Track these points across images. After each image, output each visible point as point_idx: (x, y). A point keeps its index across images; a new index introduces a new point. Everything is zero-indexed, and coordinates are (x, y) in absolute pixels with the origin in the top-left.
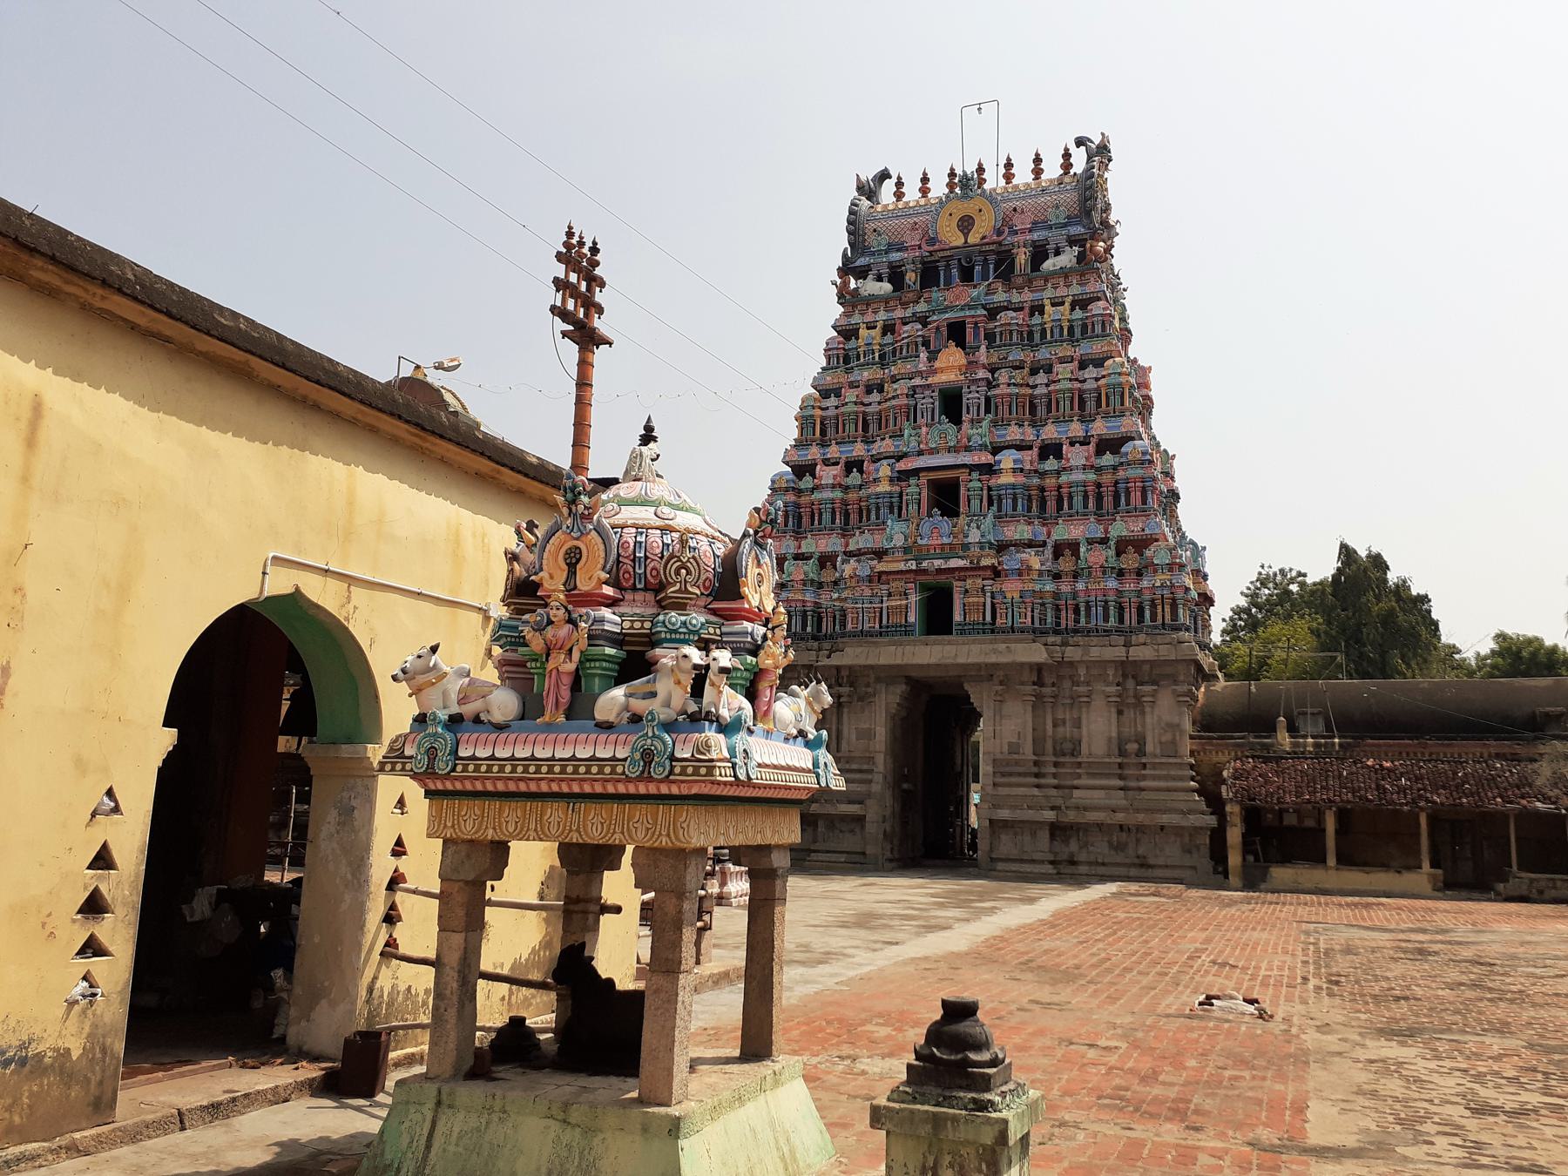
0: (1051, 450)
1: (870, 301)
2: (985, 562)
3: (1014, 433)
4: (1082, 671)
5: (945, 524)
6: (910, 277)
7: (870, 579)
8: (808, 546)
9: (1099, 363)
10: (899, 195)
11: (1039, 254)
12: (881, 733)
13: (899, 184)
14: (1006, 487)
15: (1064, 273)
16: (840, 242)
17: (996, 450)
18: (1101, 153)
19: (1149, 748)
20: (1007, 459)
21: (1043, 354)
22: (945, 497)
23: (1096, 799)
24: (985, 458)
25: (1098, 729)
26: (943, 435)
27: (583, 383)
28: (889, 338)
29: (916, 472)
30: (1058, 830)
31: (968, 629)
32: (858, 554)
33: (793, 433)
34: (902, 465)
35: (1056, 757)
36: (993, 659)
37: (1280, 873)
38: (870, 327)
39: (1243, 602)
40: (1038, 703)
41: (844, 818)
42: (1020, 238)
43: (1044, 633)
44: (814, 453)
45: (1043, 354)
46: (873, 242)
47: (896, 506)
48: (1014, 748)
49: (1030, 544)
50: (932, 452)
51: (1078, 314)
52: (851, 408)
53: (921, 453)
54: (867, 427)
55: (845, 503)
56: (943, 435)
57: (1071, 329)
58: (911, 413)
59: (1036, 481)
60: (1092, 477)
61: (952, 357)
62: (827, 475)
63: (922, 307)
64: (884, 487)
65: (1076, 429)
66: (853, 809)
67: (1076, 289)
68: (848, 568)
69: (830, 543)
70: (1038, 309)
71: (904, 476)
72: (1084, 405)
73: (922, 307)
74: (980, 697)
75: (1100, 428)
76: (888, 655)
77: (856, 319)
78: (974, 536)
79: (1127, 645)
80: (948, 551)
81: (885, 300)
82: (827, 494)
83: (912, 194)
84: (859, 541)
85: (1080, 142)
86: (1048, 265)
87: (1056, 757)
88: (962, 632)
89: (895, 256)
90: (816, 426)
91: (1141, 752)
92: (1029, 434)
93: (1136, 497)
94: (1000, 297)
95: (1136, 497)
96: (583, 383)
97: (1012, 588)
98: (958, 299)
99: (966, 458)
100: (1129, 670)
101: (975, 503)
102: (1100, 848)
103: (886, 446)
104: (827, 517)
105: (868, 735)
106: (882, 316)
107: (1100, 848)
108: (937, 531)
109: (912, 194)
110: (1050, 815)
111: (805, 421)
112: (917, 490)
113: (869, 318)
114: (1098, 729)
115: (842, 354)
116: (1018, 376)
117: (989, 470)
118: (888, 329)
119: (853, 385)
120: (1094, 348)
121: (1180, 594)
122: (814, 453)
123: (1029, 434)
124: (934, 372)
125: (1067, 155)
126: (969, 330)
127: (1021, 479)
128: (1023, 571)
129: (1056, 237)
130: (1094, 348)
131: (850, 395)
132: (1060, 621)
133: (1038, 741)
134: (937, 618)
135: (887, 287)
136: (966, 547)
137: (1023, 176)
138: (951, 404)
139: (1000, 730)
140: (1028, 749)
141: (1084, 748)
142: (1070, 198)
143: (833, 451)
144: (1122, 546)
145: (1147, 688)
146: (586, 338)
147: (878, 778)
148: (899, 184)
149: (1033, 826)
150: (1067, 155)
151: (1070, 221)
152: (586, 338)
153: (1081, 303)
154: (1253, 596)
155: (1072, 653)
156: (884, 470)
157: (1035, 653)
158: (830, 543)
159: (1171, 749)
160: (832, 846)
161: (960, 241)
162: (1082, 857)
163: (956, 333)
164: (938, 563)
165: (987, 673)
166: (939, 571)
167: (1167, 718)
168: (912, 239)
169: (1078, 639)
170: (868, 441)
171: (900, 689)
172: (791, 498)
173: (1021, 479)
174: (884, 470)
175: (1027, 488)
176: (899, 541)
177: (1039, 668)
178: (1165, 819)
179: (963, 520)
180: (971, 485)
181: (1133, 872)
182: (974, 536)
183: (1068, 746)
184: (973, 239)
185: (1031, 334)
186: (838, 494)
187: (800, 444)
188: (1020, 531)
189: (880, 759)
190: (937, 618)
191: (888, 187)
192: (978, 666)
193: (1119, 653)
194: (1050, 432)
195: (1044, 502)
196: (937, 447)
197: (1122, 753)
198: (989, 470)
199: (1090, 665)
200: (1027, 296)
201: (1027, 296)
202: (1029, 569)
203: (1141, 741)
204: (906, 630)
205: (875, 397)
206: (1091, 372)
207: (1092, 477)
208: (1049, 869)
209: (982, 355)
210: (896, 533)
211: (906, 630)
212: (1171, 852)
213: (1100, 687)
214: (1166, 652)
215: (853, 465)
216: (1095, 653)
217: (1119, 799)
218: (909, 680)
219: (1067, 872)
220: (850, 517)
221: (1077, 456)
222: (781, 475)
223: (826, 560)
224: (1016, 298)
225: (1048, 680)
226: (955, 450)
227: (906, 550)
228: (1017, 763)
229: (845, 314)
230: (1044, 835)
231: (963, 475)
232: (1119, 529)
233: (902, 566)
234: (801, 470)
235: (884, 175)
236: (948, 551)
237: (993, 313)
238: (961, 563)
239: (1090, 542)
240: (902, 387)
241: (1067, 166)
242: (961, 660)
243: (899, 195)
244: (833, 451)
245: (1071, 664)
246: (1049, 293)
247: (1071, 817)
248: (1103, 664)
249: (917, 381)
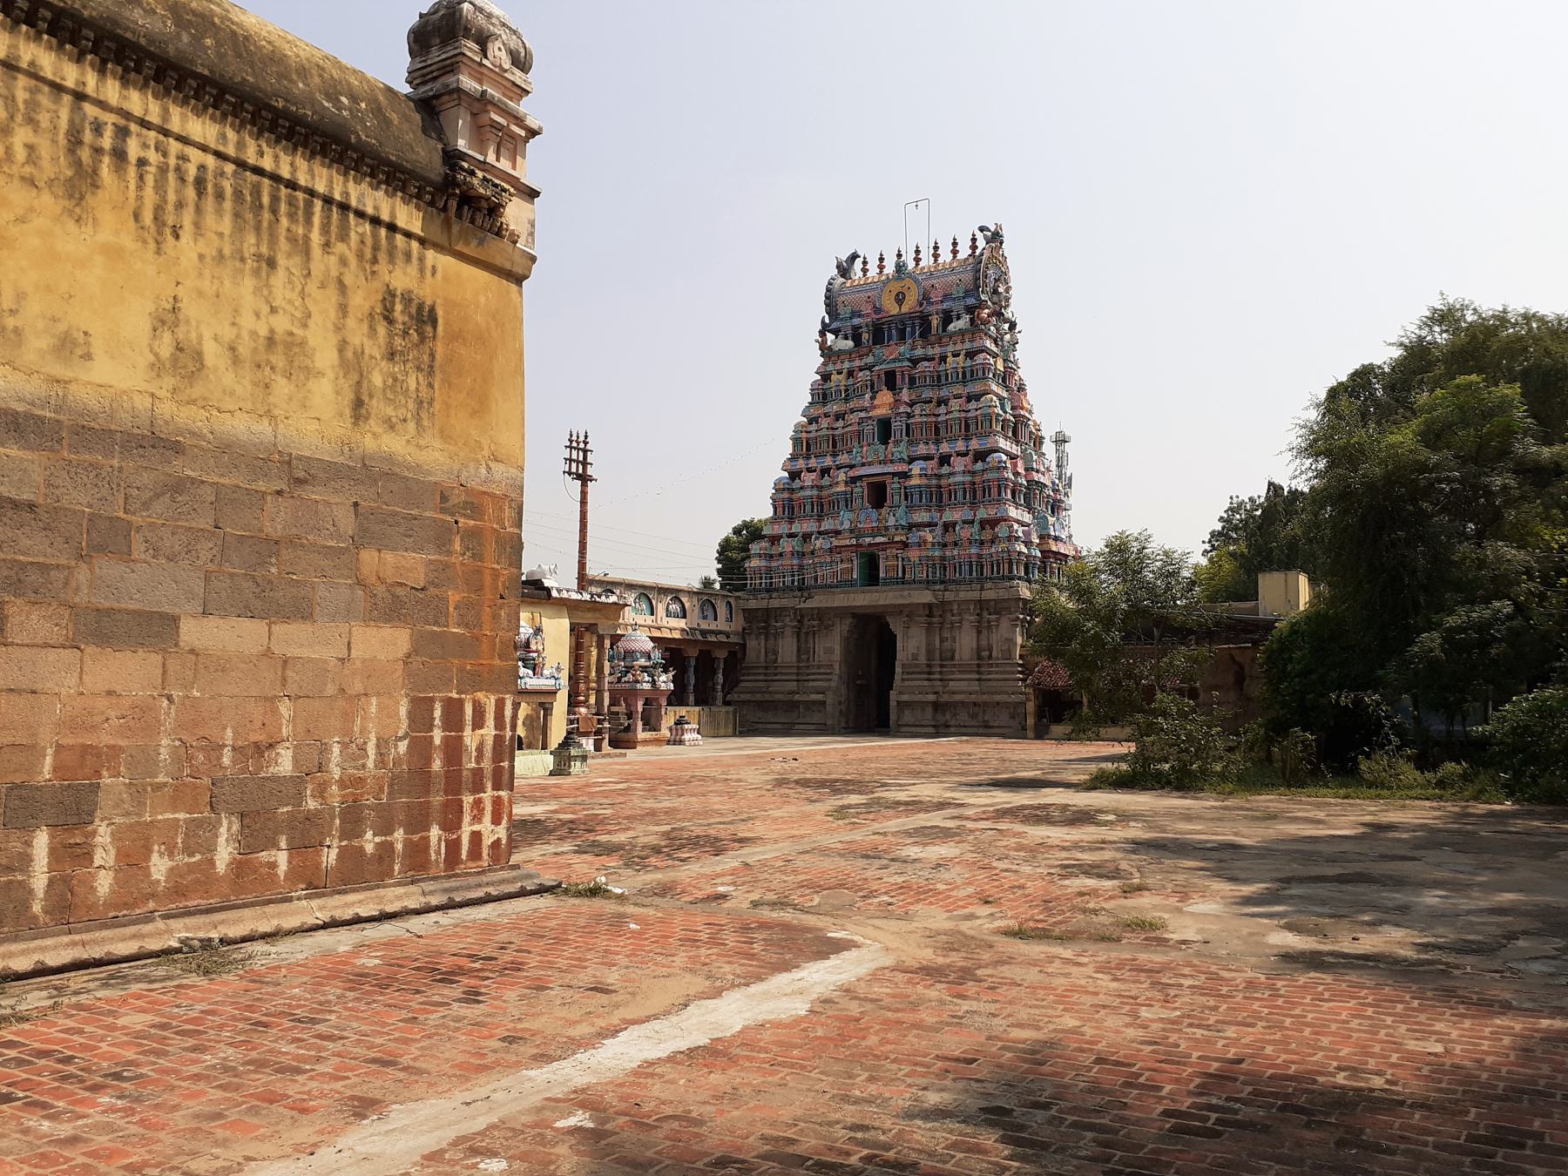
0: (944, 460)
1: (840, 353)
2: (897, 539)
3: (922, 449)
4: (955, 607)
5: (874, 514)
6: (865, 336)
7: (831, 550)
8: (796, 528)
9: (978, 397)
10: (865, 271)
11: (947, 318)
12: (838, 649)
13: (865, 263)
14: (915, 487)
15: (962, 332)
16: (821, 312)
17: (912, 460)
18: (995, 238)
19: (994, 654)
20: (916, 469)
21: (944, 393)
22: (878, 495)
23: (962, 687)
24: (903, 468)
25: (965, 643)
26: (876, 453)
27: (583, 502)
28: (851, 381)
29: (860, 478)
30: (937, 706)
31: (890, 582)
32: (826, 533)
33: (788, 449)
34: (851, 473)
35: (940, 661)
36: (900, 601)
37: (1057, 729)
38: (839, 373)
39: (1218, 526)
40: (929, 628)
41: (814, 702)
42: (932, 309)
43: (935, 583)
44: (801, 464)
45: (944, 393)
46: (844, 312)
47: (848, 501)
48: (915, 656)
49: (929, 525)
50: (870, 464)
51: (969, 363)
52: (825, 432)
53: (863, 465)
54: (835, 445)
55: (819, 497)
56: (876, 453)
57: (964, 373)
58: (859, 435)
59: (934, 482)
60: (968, 478)
61: (885, 397)
62: (808, 479)
63: (870, 359)
64: (841, 488)
65: (960, 446)
66: (820, 697)
67: (967, 345)
68: (819, 543)
69: (810, 526)
70: (943, 359)
71: (854, 480)
72: (968, 428)
73: (870, 359)
74: (896, 626)
75: (975, 444)
76: (840, 600)
77: (830, 367)
78: (891, 521)
79: (982, 589)
80: (875, 532)
81: (849, 352)
82: (808, 493)
83: (873, 270)
84: (827, 525)
85: (982, 229)
86: (951, 327)
87: (940, 661)
88: (885, 584)
89: (856, 321)
90: (804, 445)
91: (990, 657)
92: (932, 449)
93: (994, 491)
94: (919, 352)
95: (994, 491)
96: (583, 502)
97: (914, 554)
98: (893, 354)
99: (890, 469)
100: (981, 604)
101: (896, 498)
102: (963, 717)
103: (843, 459)
104: (808, 507)
105: (830, 651)
106: (847, 365)
107: (963, 717)
108: (868, 518)
109: (873, 270)
110: (931, 697)
111: (796, 441)
112: (860, 489)
113: (838, 367)
114: (965, 643)
115: (821, 395)
116: (928, 408)
117: (905, 475)
118: (850, 374)
119: (826, 415)
120: (975, 388)
121: (1015, 556)
122: (801, 464)
123: (932, 449)
124: (874, 407)
125: (974, 240)
126: (898, 376)
127: (925, 481)
128: (922, 543)
129: (958, 307)
130: (975, 388)
131: (824, 423)
132: (942, 574)
133: (930, 652)
134: (871, 575)
135: (850, 343)
136: (887, 528)
137: (946, 256)
138: (885, 427)
139: (910, 645)
140: (923, 660)
141: (957, 656)
142: (968, 277)
143: (813, 463)
144: (983, 524)
145: (993, 617)
146: (584, 479)
147: (835, 678)
148: (865, 263)
149: (923, 704)
150: (974, 240)
151: (967, 294)
152: (584, 479)
153: (971, 355)
154: (1226, 521)
155: (949, 596)
156: (842, 476)
157: (926, 597)
158: (810, 526)
159: (1008, 654)
160: (808, 720)
161: (895, 311)
162: (952, 723)
163: (890, 381)
164: (868, 540)
165: (899, 610)
166: (870, 545)
167: (1006, 635)
168: (867, 309)
169: (952, 587)
170: (834, 455)
171: (849, 621)
172: (786, 495)
173: (925, 481)
174: (842, 476)
175: (928, 486)
176: (847, 525)
177: (930, 606)
178: (998, 698)
179: (884, 511)
180: (893, 486)
181: (981, 731)
182: (891, 521)
183: (949, 654)
184: (905, 309)
185: (939, 377)
186: (815, 492)
187: (793, 458)
188: (922, 516)
189: (837, 666)
190: (871, 575)
191: (858, 264)
192: (894, 606)
193: (975, 595)
194: (945, 448)
195: (938, 496)
196: (872, 461)
197: (980, 658)
198: (905, 475)
199: (960, 603)
200: (936, 351)
201: (936, 351)
202: (925, 542)
203: (990, 650)
204: (851, 583)
205: (840, 423)
206: (973, 405)
207: (968, 478)
208: (932, 730)
209: (905, 395)
210: (845, 520)
211: (851, 583)
212: (1003, 718)
213: (967, 617)
214: (1003, 594)
215: (825, 471)
216: (962, 595)
217: (975, 686)
218: (854, 615)
219: (940, 730)
220: (822, 507)
221: (959, 464)
222: (780, 479)
223: (806, 537)
224: (930, 352)
225: (936, 613)
226: (884, 462)
227: (852, 531)
228: (916, 666)
229: (824, 364)
230: (929, 710)
231: (888, 480)
232: (982, 513)
233: (847, 542)
234: (794, 475)
235: (854, 257)
236: (875, 532)
237: (915, 362)
238: (882, 539)
239: (965, 522)
240: (854, 418)
241: (974, 247)
242: (881, 603)
243: (865, 271)
244: (813, 463)
245: (950, 602)
246: (951, 348)
247: (945, 698)
248: (967, 602)
249: (863, 415)
